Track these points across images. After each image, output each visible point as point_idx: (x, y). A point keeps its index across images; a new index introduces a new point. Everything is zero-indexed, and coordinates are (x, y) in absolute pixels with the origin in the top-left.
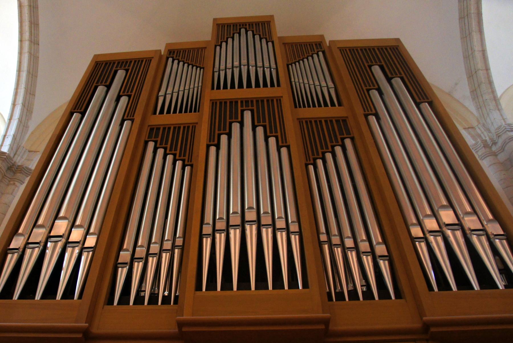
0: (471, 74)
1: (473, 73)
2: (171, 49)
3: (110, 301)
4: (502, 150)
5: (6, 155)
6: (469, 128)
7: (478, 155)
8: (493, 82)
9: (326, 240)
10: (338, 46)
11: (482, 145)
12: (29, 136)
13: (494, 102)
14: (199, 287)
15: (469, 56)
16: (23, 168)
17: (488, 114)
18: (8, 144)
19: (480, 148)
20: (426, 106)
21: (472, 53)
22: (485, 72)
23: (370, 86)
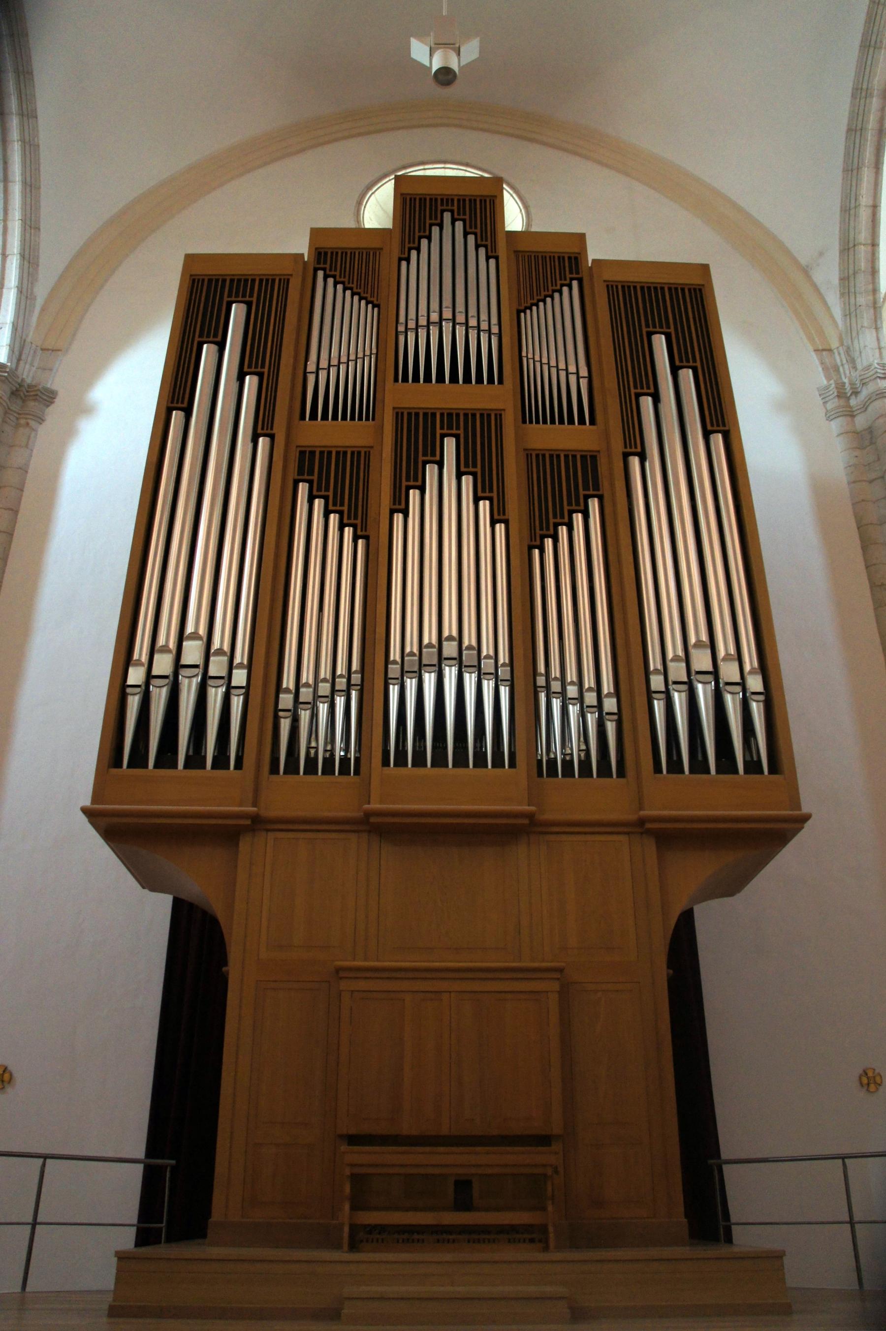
0: (847, 248)
1: (851, 245)
2: (322, 245)
3: (274, 769)
4: (862, 410)
5: (8, 370)
6: (823, 350)
7: (826, 409)
8: (878, 271)
9: (544, 685)
10: (605, 279)
11: (836, 394)
12: (39, 318)
13: (872, 311)
14: (386, 762)
15: (850, 209)
16: (39, 390)
17: (858, 334)
18: (5, 344)
19: (831, 397)
20: (718, 440)
21: (856, 207)
22: (869, 248)
23: (655, 327)
